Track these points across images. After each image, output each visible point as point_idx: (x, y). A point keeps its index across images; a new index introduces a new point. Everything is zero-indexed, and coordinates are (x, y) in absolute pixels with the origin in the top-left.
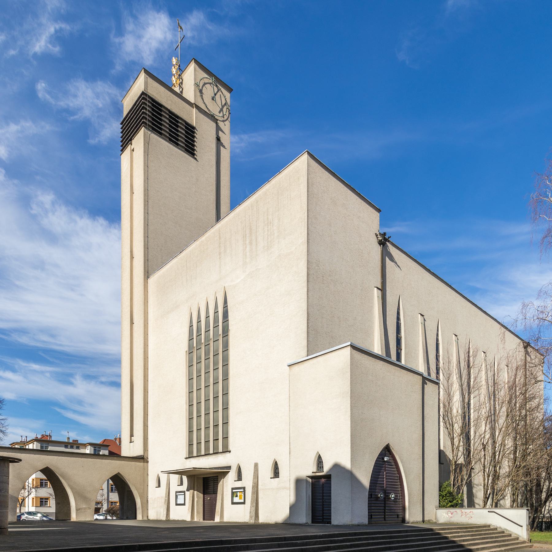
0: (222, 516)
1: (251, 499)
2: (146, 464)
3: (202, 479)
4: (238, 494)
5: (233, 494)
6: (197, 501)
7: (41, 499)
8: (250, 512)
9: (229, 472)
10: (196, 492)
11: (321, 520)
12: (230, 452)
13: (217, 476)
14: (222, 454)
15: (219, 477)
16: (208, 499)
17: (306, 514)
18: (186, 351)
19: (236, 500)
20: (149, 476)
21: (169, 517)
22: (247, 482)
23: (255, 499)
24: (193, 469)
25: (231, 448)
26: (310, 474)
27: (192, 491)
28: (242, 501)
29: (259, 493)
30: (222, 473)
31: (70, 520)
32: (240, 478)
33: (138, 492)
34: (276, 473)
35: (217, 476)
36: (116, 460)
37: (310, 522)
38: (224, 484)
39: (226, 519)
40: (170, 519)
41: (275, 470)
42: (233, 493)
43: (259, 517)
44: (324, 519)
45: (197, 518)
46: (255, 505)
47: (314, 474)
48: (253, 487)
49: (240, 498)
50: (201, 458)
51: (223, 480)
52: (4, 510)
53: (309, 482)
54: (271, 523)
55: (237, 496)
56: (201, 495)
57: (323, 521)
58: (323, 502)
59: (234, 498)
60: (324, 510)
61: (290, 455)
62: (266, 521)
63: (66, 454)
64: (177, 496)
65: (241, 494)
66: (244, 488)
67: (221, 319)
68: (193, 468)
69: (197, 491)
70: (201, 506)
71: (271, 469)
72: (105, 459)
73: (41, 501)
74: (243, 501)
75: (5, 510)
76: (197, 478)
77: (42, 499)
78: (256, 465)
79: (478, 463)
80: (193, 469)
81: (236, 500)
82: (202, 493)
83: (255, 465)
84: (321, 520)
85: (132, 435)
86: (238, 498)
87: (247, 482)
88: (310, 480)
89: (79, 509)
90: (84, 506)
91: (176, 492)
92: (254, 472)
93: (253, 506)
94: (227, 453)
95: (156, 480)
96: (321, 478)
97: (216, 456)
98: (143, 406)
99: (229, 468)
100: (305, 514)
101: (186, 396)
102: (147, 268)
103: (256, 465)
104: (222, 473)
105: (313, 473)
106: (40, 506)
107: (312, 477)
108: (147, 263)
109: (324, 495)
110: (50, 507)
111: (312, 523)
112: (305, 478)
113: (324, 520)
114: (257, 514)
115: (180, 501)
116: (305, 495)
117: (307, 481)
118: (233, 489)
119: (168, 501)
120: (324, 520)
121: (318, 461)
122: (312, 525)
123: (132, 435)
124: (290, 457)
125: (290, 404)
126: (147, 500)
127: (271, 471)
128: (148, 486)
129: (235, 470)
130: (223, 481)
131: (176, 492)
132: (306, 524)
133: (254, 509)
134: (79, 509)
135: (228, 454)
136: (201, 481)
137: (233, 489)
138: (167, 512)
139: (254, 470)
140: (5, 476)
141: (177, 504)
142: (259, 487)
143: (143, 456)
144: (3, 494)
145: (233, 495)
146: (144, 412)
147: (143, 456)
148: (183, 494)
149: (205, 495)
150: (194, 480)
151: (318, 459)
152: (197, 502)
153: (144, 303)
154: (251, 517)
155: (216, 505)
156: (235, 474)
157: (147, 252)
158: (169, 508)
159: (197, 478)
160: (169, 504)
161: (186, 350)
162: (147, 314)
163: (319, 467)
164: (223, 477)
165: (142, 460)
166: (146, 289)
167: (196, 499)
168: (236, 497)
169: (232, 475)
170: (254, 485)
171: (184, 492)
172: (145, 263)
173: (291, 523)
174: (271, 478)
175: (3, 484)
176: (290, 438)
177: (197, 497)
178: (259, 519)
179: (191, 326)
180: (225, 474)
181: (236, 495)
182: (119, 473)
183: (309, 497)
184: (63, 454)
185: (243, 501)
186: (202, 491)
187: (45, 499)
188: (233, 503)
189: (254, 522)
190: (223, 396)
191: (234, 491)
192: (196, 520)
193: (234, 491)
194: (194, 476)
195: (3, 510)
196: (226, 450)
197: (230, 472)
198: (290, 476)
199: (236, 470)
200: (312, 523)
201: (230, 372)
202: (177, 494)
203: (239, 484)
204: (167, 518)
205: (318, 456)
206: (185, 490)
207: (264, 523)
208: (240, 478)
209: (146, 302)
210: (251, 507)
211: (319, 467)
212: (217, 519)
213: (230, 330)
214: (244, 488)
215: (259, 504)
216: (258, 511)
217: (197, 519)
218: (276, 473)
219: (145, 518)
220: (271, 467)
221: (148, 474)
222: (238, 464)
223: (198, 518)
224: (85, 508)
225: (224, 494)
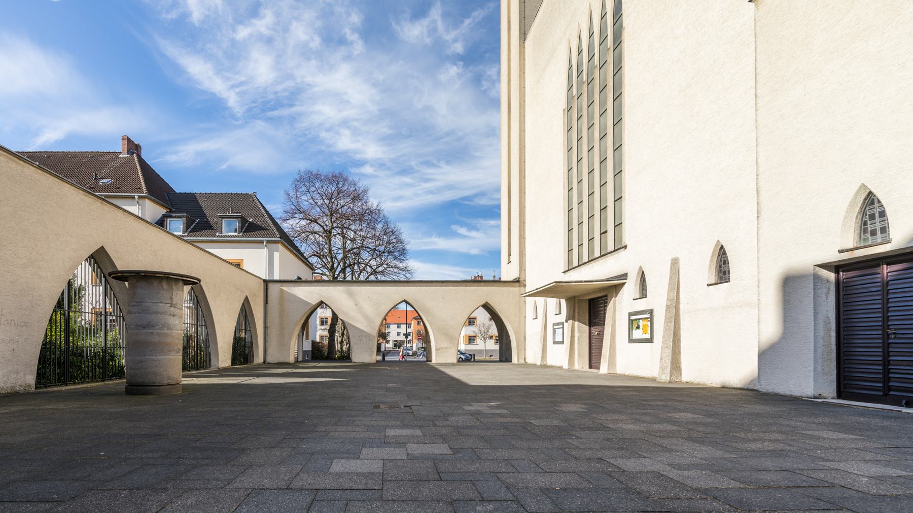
0: (612, 363)
1: (664, 332)
2: (523, 288)
3: (588, 301)
4: (641, 323)
5: (633, 324)
6: (578, 337)
7: (469, 337)
8: (661, 359)
9: (624, 284)
10: (576, 323)
11: (881, 393)
12: (625, 247)
13: (606, 296)
14: (613, 253)
15: (609, 296)
16: (596, 333)
17: (815, 371)
18: (564, 110)
19: (637, 334)
20: (527, 305)
21: (546, 361)
22: (657, 300)
23: (672, 332)
24: (554, 284)
25: (626, 240)
26: (833, 256)
27: (570, 322)
28: (648, 336)
29: (681, 320)
30: (613, 288)
31: (431, 361)
32: (643, 293)
33: (512, 326)
34: (723, 273)
35: (606, 296)
36: (483, 286)
37: (829, 391)
38: (617, 307)
39: (620, 370)
40: (546, 363)
41: (721, 266)
42: (631, 322)
43: (681, 370)
44: (890, 388)
45: (579, 364)
46: (671, 344)
47: (845, 256)
48: (668, 307)
49: (645, 332)
50: (583, 268)
51: (614, 299)
52: (159, 356)
53: (828, 281)
54: (711, 385)
55: (638, 327)
56: (587, 328)
57: (886, 395)
58: (888, 338)
59: (634, 330)
60: (891, 362)
61: (757, 221)
62: (697, 380)
63: (425, 284)
64: (555, 331)
65: (645, 323)
66: (651, 312)
67: (611, 19)
68: (555, 282)
69: (578, 321)
70: (586, 346)
71: (710, 266)
72: (470, 286)
73: (469, 339)
74: (649, 338)
75: (161, 357)
76: (579, 300)
77: (471, 337)
78: (675, 263)
79: (376, 400)
80: (554, 284)
81: (637, 334)
82: (588, 324)
83: (672, 263)
84: (881, 393)
85: (509, 255)
86: (640, 331)
87: (657, 300)
88: (832, 276)
89: (439, 349)
90: (445, 346)
91: (553, 324)
92: (671, 277)
93: (667, 347)
94: (621, 251)
95: (533, 308)
96: (878, 266)
97: (603, 260)
98: (518, 213)
99: (625, 276)
100: (812, 372)
101: (564, 178)
102: (523, 29)
103: (675, 263)
104: (613, 288)
105: (841, 251)
106: (469, 343)
107: (837, 267)
108: (523, 22)
109: (889, 314)
110: (477, 344)
111: (839, 396)
112: (811, 269)
113: (892, 393)
114: (677, 363)
115: (559, 338)
116: (812, 317)
117: (816, 278)
118: (630, 314)
119: (544, 338)
120: (892, 393)
121: (864, 214)
122: (841, 406)
123: (509, 255)
124: (758, 224)
125: (759, 91)
126: (525, 337)
127: (710, 269)
128: (525, 317)
129: (635, 278)
130: (615, 300)
131: (554, 325)
132: (815, 398)
133: (669, 352)
134: (439, 349)
135: (622, 253)
136: (586, 306)
137: (630, 314)
138: (542, 354)
139: (670, 274)
140: (162, 303)
141: (555, 343)
142: (682, 307)
143: (519, 278)
144: (157, 331)
145: (632, 325)
146: (520, 219)
147: (519, 278)
148: (561, 326)
149: (592, 328)
150: (574, 306)
151: (861, 208)
152: (578, 339)
153: (520, 75)
154: (662, 369)
155: (602, 344)
156: (634, 287)
157: (523, 8)
158: (546, 348)
159: (579, 300)
160: (546, 342)
161: (564, 108)
162: (523, 89)
163: (865, 231)
164: (614, 295)
165: (517, 284)
166: (522, 56)
167: (577, 335)
168: (638, 330)
169: (630, 289)
170: (669, 303)
171: (562, 324)
172: (520, 23)
173: (764, 391)
174: (708, 285)
175: (159, 315)
176: (759, 177)
177: (579, 331)
178: (681, 374)
179: (570, 68)
180: (617, 288)
181: (636, 325)
182: (487, 302)
183: (827, 324)
184: (422, 284)
185: (649, 338)
186: (587, 321)
187: (473, 337)
188: (631, 341)
189: (668, 379)
190: (615, 154)
191: (633, 318)
192: (577, 367)
193: (633, 318)
194: (574, 297)
195: (158, 357)
196: (620, 247)
197: (626, 284)
198: (759, 273)
199: (636, 280)
200: (839, 396)
201: (624, 104)
202: (555, 327)
203: (642, 305)
204: (543, 362)
205: (864, 196)
206: (564, 320)
207: (692, 383)
208: (643, 293)
209: (522, 73)
210: (662, 349)
211: (865, 231)
212: (604, 369)
213: (624, 27)
214: (651, 312)
215: (682, 342)
216: (680, 357)
217: (578, 366)
218: (723, 273)
219: (522, 361)
220: (709, 261)
221: (525, 302)
222: (641, 267)
223: (581, 364)
224: (446, 348)
225: (617, 324)
